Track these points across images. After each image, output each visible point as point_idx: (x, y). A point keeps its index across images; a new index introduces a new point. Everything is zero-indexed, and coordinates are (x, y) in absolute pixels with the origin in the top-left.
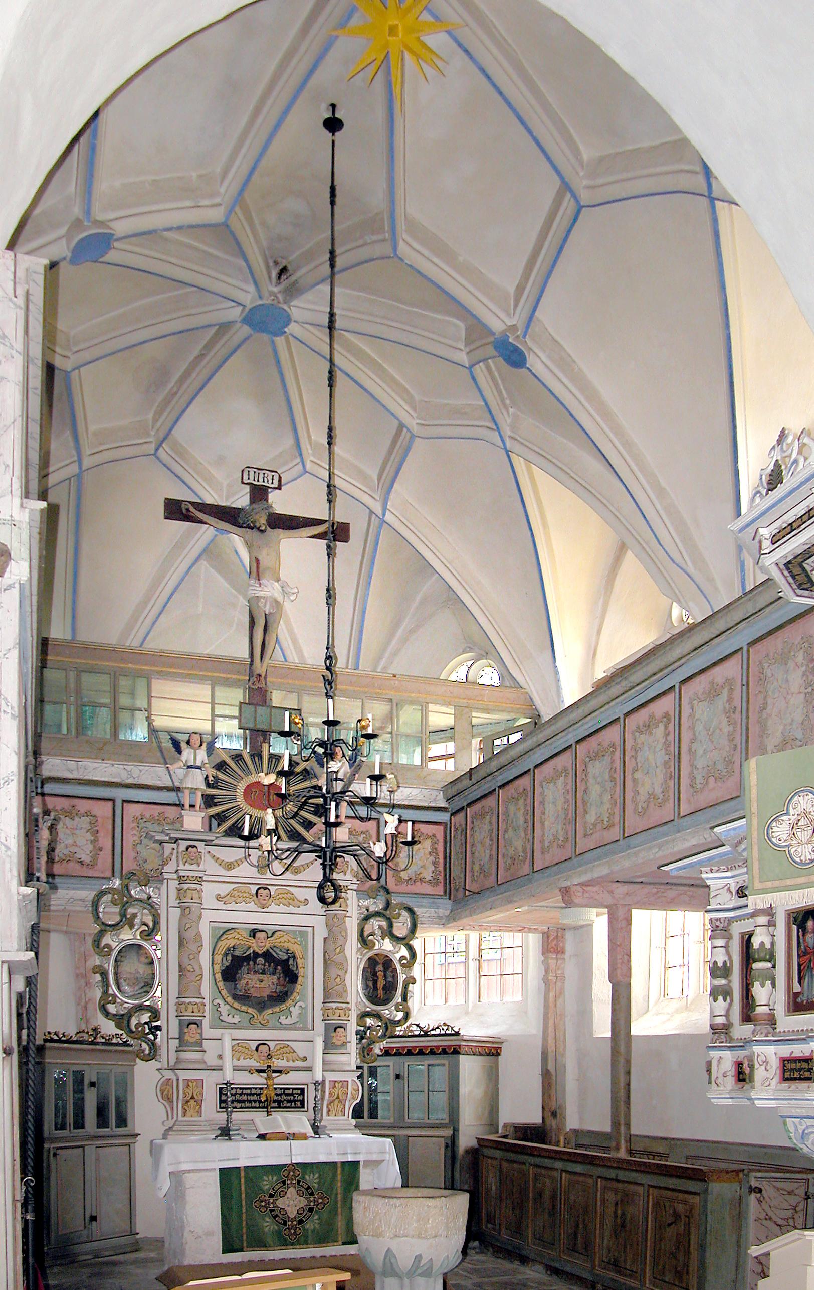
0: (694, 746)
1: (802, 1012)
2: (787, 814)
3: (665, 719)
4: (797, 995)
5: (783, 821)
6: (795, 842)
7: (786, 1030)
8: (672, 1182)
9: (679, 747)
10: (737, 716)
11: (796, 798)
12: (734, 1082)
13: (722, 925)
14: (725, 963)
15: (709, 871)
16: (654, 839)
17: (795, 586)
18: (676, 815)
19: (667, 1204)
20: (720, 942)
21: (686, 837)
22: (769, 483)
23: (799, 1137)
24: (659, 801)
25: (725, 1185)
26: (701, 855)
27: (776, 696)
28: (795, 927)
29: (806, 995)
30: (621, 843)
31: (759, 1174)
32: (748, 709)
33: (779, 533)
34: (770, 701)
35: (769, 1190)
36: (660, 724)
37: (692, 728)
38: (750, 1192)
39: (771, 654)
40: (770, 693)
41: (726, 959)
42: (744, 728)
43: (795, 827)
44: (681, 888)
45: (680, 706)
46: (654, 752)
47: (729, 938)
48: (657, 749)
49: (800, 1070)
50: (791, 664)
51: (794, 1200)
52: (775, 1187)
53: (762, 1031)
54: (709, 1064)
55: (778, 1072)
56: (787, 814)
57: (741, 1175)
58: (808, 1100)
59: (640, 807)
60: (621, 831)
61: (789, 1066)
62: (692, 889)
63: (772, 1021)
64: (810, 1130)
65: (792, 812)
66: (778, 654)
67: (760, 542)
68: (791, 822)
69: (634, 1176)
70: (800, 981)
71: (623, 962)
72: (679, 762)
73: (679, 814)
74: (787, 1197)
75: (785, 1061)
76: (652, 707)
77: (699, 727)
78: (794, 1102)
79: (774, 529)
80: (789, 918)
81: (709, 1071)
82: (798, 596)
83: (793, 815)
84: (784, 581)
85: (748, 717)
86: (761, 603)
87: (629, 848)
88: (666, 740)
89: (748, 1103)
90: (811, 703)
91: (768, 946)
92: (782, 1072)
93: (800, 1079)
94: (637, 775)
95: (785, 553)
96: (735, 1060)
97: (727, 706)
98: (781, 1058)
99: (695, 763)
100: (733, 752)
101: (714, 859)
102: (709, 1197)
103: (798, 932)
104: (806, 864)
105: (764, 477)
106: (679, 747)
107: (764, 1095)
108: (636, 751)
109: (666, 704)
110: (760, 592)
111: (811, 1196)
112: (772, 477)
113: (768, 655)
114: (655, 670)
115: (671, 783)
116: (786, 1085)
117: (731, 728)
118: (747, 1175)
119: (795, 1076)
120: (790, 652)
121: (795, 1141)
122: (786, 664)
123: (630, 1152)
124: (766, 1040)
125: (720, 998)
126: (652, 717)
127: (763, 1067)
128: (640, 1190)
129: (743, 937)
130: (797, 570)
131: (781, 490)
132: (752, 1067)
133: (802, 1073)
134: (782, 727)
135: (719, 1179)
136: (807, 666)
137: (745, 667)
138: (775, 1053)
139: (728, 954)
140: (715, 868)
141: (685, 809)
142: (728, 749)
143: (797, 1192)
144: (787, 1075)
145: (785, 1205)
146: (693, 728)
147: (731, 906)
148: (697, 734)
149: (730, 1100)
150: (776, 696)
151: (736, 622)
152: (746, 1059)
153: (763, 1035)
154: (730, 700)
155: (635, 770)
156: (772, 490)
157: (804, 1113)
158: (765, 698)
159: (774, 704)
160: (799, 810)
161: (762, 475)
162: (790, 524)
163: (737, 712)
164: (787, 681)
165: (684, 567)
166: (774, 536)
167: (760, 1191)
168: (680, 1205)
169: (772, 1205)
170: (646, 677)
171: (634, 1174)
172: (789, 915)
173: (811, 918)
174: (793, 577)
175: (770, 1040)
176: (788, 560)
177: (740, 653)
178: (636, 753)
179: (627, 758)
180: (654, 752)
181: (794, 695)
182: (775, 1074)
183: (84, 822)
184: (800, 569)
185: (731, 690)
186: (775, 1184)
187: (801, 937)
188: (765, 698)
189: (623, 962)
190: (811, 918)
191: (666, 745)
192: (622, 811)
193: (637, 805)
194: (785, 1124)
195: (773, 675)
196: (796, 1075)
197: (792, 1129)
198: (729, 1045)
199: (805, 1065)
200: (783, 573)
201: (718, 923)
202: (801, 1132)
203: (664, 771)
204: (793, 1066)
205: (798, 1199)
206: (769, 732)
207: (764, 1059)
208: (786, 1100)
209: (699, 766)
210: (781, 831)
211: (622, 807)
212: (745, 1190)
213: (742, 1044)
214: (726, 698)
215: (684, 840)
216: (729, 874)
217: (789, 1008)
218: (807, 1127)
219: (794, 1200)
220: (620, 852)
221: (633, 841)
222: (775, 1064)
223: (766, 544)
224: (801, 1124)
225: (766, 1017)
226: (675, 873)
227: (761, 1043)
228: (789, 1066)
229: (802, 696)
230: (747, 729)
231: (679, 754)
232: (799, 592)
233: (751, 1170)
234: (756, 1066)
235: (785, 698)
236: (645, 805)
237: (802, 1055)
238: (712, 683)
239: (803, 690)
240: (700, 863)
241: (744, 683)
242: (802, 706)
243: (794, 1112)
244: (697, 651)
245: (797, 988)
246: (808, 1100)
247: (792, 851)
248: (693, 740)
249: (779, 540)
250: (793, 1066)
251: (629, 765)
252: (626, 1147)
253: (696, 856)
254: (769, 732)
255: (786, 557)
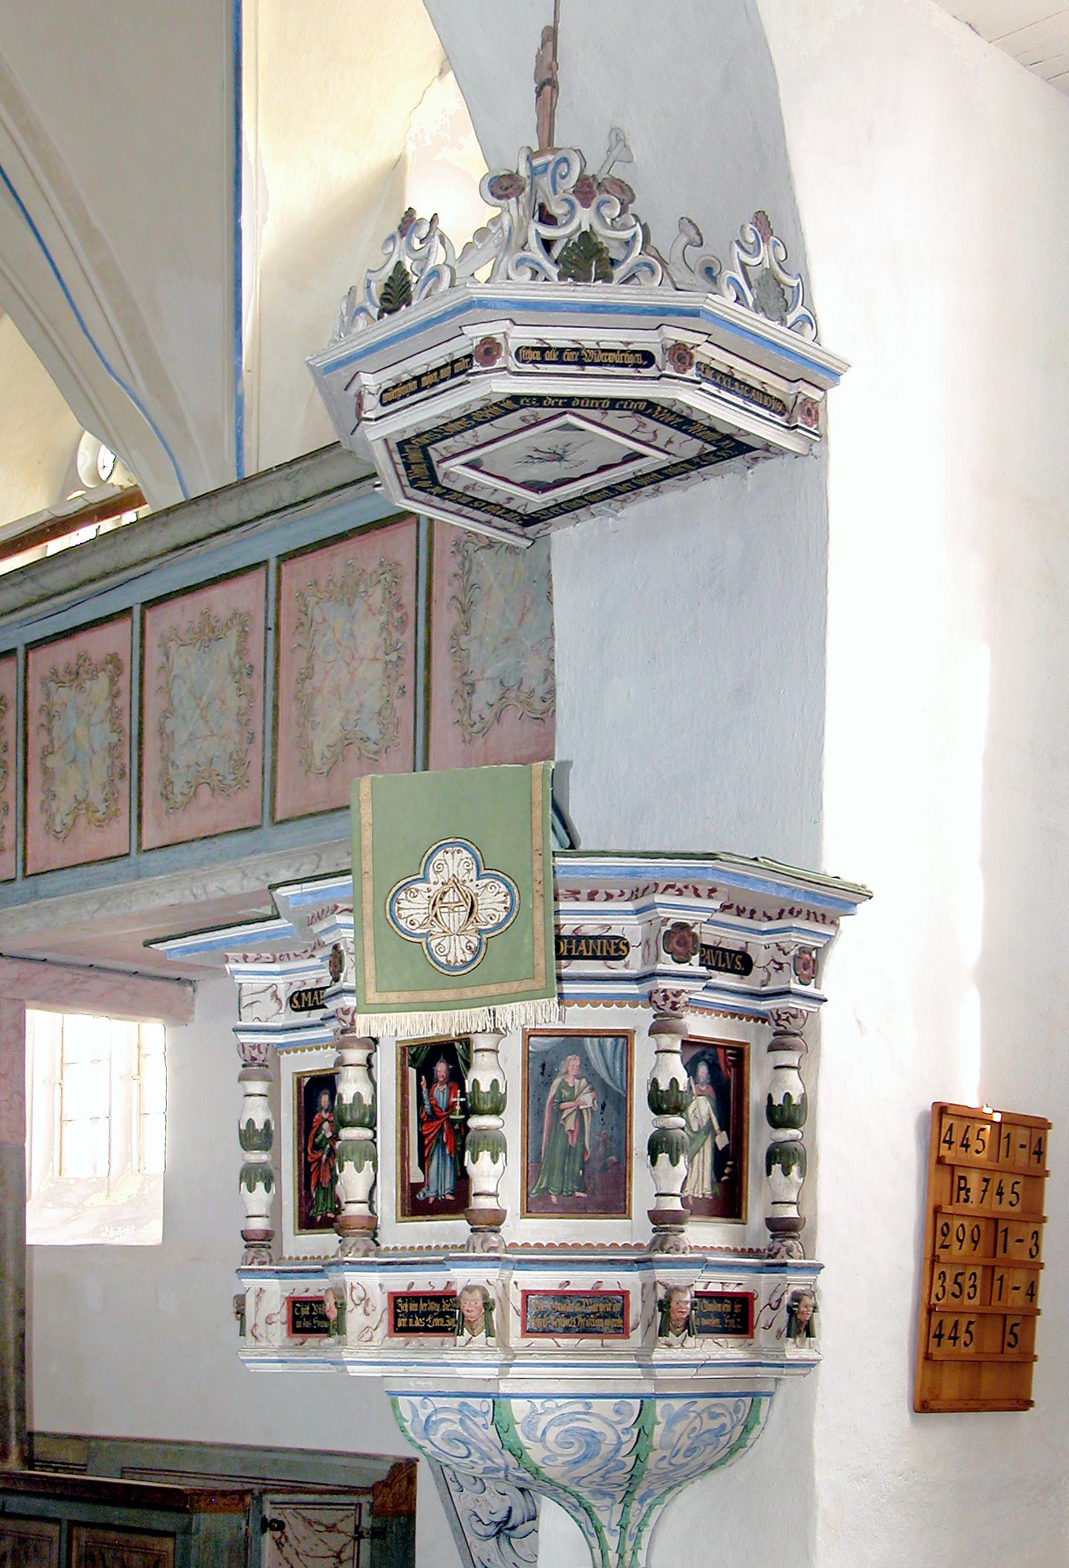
0: (169, 727)
1: (428, 1217)
2: (425, 879)
3: (110, 666)
4: (417, 1187)
5: (417, 891)
6: (437, 929)
7: (399, 1246)
8: (116, 1515)
9: (141, 723)
10: (256, 683)
11: (440, 855)
12: (285, 1334)
13: (262, 1057)
14: (267, 1124)
15: (241, 959)
16: (88, 886)
17: (405, 481)
18: (134, 845)
19: (109, 1555)
20: (257, 1087)
21: (157, 890)
22: (384, 299)
23: (420, 1429)
24: (99, 815)
25: (221, 1517)
26: (233, 929)
27: (331, 657)
28: (412, 1072)
29: (433, 1189)
30: (19, 884)
31: (279, 1498)
32: (277, 672)
33: (394, 387)
34: (319, 666)
35: (295, 1526)
36: (101, 675)
37: (166, 690)
38: (264, 1530)
39: (323, 583)
40: (319, 651)
41: (270, 1117)
42: (270, 705)
43: (439, 904)
44: (117, 977)
45: (142, 646)
46: (89, 725)
47: (273, 1080)
48: (94, 720)
49: (425, 1315)
50: (359, 605)
51: (336, 1541)
52: (304, 1519)
53: (360, 1245)
54: (240, 1301)
55: (386, 1317)
56: (425, 879)
57: (248, 1499)
58: (448, 1365)
59: (58, 821)
60: (20, 865)
61: (404, 1307)
62: (134, 979)
63: (372, 1229)
64: (440, 1416)
65: (432, 877)
66: (335, 585)
67: (359, 396)
68: (431, 894)
69: (36, 1505)
70: (423, 1163)
71: (11, 1107)
72: (140, 748)
73: (139, 845)
74: (326, 1536)
75: (397, 1300)
76: (84, 640)
77: (181, 691)
78: (415, 1368)
79: (386, 378)
80: (403, 1056)
81: (240, 1313)
82: (407, 498)
83: (435, 883)
84: (391, 471)
85: (276, 688)
86: (308, 488)
87: (35, 895)
88: (113, 705)
89: (334, 1369)
90: (396, 679)
91: (367, 1101)
92: (392, 1317)
93: (426, 1330)
94: (51, 762)
95: (405, 425)
96: (287, 1295)
97: (236, 663)
98: (390, 1293)
99: (172, 755)
100: (246, 746)
101: (256, 939)
102: (194, 1541)
103: (419, 1080)
104: (455, 968)
105: (373, 285)
106: (141, 723)
107: (363, 1356)
108: (51, 717)
109: (115, 638)
110: (308, 469)
111: (365, 1534)
112: (389, 290)
113: (316, 583)
114: (96, 572)
115: (123, 786)
116: (400, 1339)
117: (244, 702)
118: (259, 1500)
119: (417, 1324)
120: (358, 585)
121: (412, 1434)
122: (350, 605)
123: (29, 1460)
124: (367, 1263)
125: (260, 1185)
126: (83, 657)
127: (360, 1309)
128: (52, 1530)
129: (299, 1081)
130: (415, 456)
131: (405, 318)
132: (341, 1307)
133: (429, 1319)
134: (342, 714)
135: (211, 1508)
136: (390, 614)
137: (272, 596)
138: (381, 1286)
139: (274, 1106)
140: (252, 955)
141: (151, 837)
142: (237, 738)
143: (341, 1526)
144: (402, 1322)
145: (322, 1550)
146: (169, 691)
147: (279, 1024)
148: (176, 703)
149: (280, 1365)
150: (331, 657)
151: (258, 513)
152: (330, 1293)
153: (361, 1253)
154: (241, 651)
155: (47, 752)
156: (390, 312)
157: (431, 1386)
158: (309, 659)
159: (327, 673)
160: (445, 876)
161: (369, 282)
162: (418, 378)
163: (255, 674)
164: (352, 635)
165: (129, 383)
166: (386, 391)
167: (281, 1526)
168: (135, 1556)
169: (300, 1550)
170: (75, 583)
171: (39, 1503)
172: (403, 1049)
173: (442, 1058)
174: (407, 466)
175: (372, 1263)
176: (405, 437)
177: (262, 569)
178: (50, 721)
179: (32, 729)
180: (89, 725)
181: (365, 662)
182: (381, 1321)
183: (63, 694)
184: (421, 455)
185: (244, 634)
186: (304, 1513)
187: (424, 1089)
188: (309, 659)
189: (11, 1107)
190: (442, 1058)
191: (114, 715)
192: (20, 823)
193: (52, 816)
194: (395, 1405)
195: (324, 620)
196: (418, 1322)
197: (407, 1413)
198: (276, 1268)
199: (434, 1306)
200: (392, 458)
201: (255, 1053)
202: (424, 1419)
203: (108, 761)
204: (413, 1307)
205: (343, 1539)
206: (318, 719)
207: (362, 1295)
208: (401, 1364)
209: (181, 760)
210: (414, 908)
211: (20, 816)
212: (255, 1525)
213: (320, 1267)
214: (233, 648)
215: (152, 892)
216: (276, 967)
217: (403, 1209)
218: (436, 1411)
219: (336, 1541)
220: (17, 903)
221: (45, 883)
222: (380, 1303)
223: (371, 405)
224: (424, 1406)
225: (365, 1223)
226: (178, 957)
227: (357, 1267)
228: (404, 1307)
229: (379, 666)
230: (276, 707)
231: (141, 734)
232: (411, 492)
233: (265, 1492)
234: (350, 1306)
235: (348, 665)
236: (69, 820)
237: (429, 1289)
238: (206, 614)
239: (381, 654)
240: (227, 943)
241: (271, 624)
242: (379, 683)
243: (412, 1386)
244: (181, 552)
245: (416, 1176)
246: (448, 1365)
247: (433, 944)
248: (168, 713)
249: (394, 401)
250: (413, 1307)
251: (37, 741)
252: (21, 1451)
253: (222, 932)
254: (318, 719)
255: (404, 431)
